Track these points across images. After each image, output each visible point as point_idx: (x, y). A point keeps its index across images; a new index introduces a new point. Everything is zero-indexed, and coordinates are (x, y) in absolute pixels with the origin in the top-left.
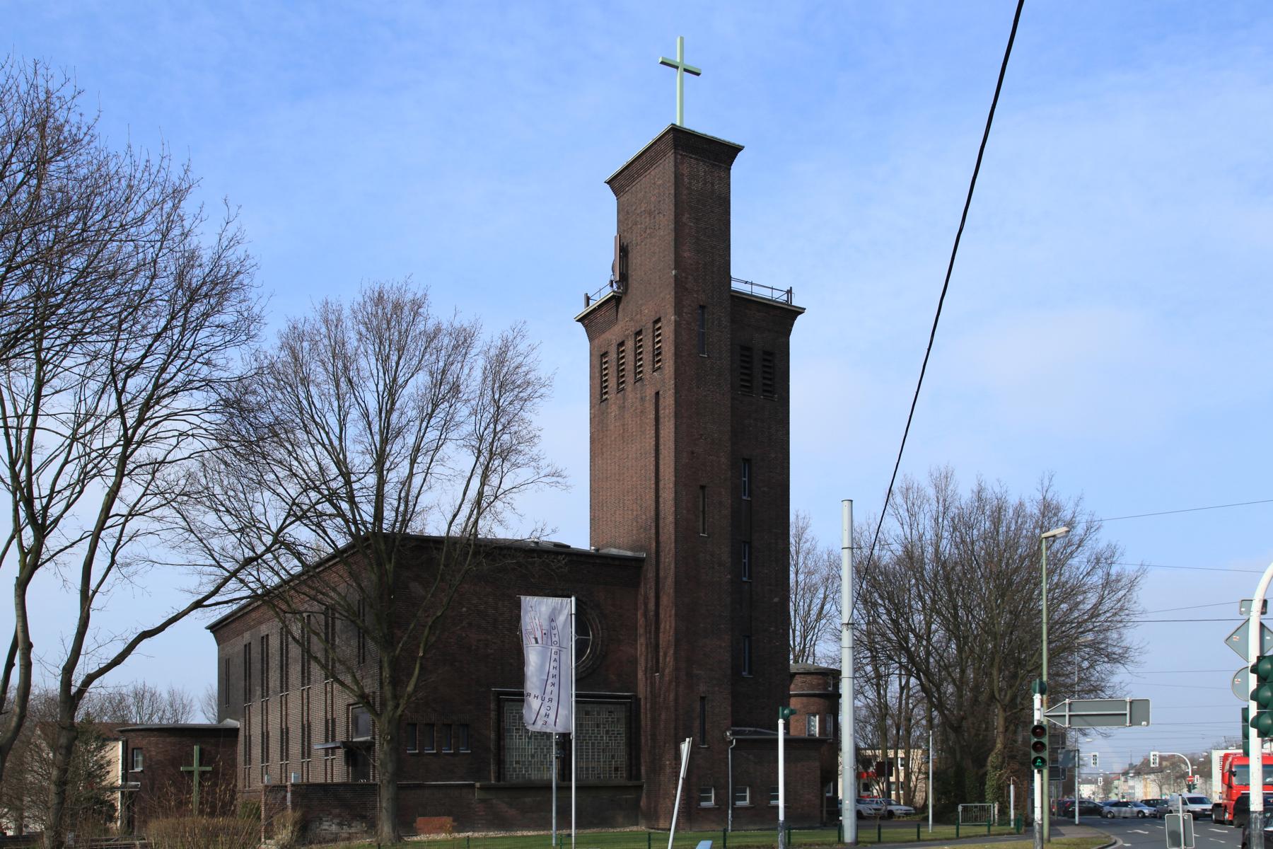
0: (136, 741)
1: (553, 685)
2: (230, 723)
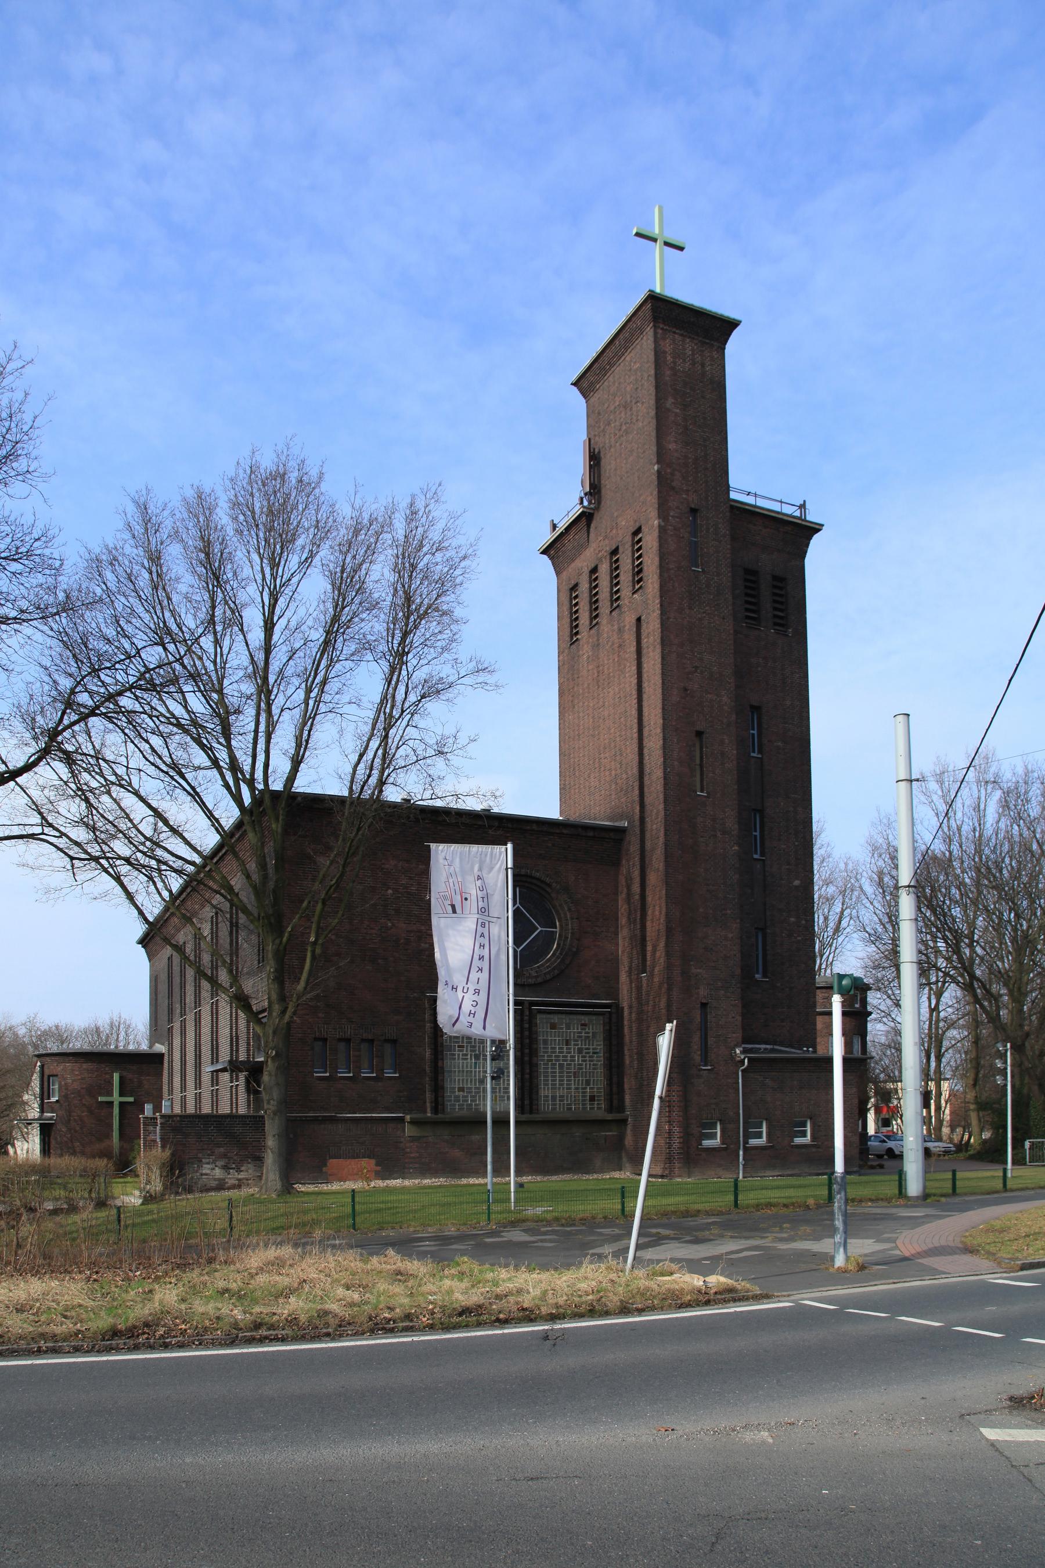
0: (53, 1067)
1: (481, 970)
2: (160, 1048)
